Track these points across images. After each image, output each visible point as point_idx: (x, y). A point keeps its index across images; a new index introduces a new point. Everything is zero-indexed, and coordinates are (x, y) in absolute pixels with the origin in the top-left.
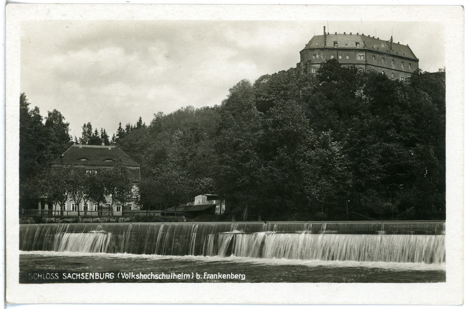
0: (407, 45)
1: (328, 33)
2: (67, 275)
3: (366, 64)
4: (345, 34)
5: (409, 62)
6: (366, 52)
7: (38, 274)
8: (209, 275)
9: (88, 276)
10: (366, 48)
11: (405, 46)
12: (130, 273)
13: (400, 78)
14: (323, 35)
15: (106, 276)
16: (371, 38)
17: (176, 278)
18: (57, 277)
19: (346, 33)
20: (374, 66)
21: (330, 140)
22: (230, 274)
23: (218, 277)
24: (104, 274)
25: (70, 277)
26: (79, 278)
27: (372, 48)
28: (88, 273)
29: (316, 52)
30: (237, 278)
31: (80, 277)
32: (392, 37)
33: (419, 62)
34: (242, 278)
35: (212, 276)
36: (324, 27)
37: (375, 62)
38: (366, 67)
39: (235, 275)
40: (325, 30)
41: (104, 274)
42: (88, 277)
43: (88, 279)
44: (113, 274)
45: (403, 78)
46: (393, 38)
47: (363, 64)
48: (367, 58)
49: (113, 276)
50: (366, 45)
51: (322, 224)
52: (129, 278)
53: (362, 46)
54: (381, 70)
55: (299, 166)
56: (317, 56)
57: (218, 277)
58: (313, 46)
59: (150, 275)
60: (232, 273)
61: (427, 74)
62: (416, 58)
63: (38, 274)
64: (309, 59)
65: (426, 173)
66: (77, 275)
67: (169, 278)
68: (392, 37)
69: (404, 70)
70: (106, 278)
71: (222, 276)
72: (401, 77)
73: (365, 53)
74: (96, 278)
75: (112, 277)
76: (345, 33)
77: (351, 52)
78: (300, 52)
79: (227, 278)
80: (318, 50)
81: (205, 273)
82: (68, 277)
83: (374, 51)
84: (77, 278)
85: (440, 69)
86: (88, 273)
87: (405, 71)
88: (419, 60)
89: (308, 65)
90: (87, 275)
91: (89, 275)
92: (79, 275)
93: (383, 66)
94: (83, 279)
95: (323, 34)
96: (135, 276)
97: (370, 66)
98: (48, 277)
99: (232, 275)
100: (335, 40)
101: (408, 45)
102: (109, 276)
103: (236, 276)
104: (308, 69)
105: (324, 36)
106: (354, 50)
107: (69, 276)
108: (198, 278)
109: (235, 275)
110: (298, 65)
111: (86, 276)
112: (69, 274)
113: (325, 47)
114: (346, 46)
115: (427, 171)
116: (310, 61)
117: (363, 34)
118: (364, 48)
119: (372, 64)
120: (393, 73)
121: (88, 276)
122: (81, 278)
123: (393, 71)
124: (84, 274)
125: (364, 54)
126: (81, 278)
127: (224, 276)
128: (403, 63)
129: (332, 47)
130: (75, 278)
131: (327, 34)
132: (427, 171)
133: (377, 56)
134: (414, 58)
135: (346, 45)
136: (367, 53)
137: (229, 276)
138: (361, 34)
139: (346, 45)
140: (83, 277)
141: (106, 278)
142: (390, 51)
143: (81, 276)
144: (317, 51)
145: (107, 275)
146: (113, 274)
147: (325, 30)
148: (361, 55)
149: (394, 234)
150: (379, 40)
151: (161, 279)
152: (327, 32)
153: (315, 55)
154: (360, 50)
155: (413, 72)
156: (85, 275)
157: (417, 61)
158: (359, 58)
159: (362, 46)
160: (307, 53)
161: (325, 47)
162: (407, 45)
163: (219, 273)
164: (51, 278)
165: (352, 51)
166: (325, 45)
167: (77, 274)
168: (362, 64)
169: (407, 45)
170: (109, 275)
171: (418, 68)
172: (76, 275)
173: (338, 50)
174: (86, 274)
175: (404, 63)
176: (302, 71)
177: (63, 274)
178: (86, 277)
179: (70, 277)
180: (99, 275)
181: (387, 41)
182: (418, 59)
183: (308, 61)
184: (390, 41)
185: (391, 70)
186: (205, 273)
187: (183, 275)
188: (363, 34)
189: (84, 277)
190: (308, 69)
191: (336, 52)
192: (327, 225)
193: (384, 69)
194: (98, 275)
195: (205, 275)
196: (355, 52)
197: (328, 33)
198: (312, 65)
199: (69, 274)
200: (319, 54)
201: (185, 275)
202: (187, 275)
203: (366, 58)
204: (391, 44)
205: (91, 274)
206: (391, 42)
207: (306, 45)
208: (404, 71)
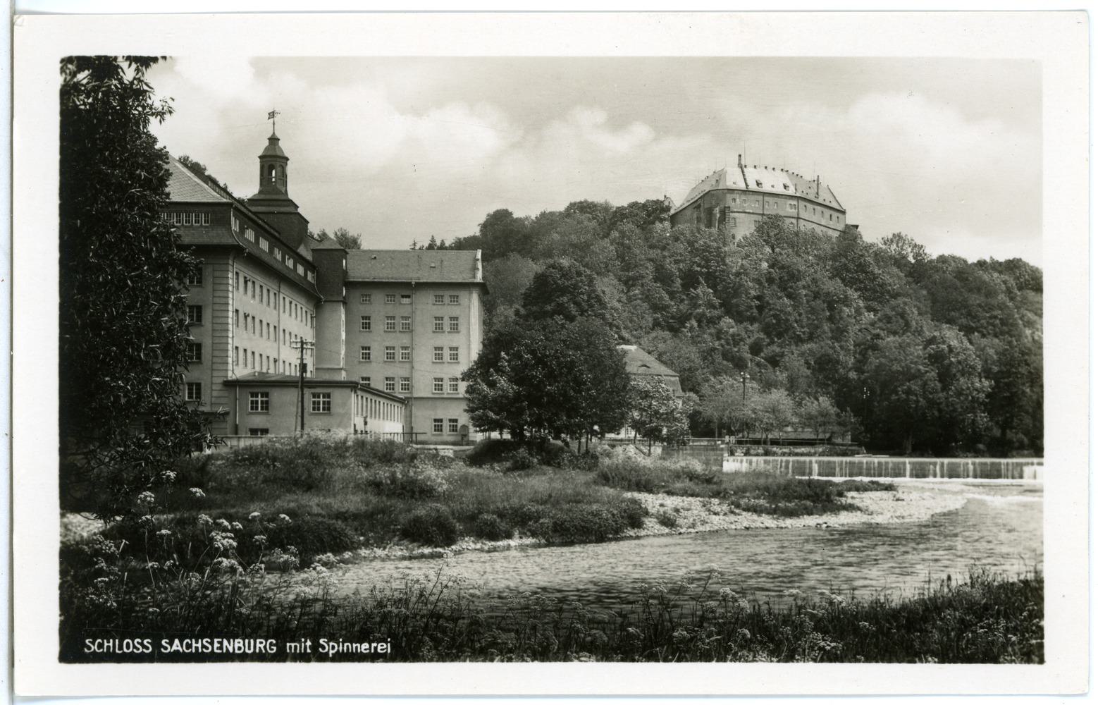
2: (171, 644)
7: (105, 641)
15: (258, 645)
18: (148, 648)
25: (180, 648)
26: (200, 651)
28: (220, 640)
30: (368, 651)
31: (202, 648)
36: (740, 156)
40: (740, 160)
42: (221, 648)
43: (219, 651)
49: (275, 648)
52: (338, 650)
63: (105, 641)
70: (257, 651)
74: (237, 651)
84: (194, 651)
86: (220, 640)
91: (221, 643)
92: (199, 645)
102: (265, 647)
111: (216, 645)
112: (177, 641)
122: (204, 650)
124: (140, 641)
126: (204, 650)
130: (101, 650)
135: (773, 186)
137: (357, 647)
139: (773, 186)
140: (207, 648)
143: (203, 646)
147: (740, 160)
149: (353, 547)
153: (734, 200)
154: (791, 197)
164: (135, 651)
167: (194, 640)
168: (793, 218)
172: (192, 644)
173: (764, 194)
174: (216, 640)
177: (87, 641)
179: (180, 648)
187: (343, 646)
189: (210, 647)
191: (760, 198)
194: (241, 645)
199: (177, 641)
201: (346, 645)
205: (225, 643)
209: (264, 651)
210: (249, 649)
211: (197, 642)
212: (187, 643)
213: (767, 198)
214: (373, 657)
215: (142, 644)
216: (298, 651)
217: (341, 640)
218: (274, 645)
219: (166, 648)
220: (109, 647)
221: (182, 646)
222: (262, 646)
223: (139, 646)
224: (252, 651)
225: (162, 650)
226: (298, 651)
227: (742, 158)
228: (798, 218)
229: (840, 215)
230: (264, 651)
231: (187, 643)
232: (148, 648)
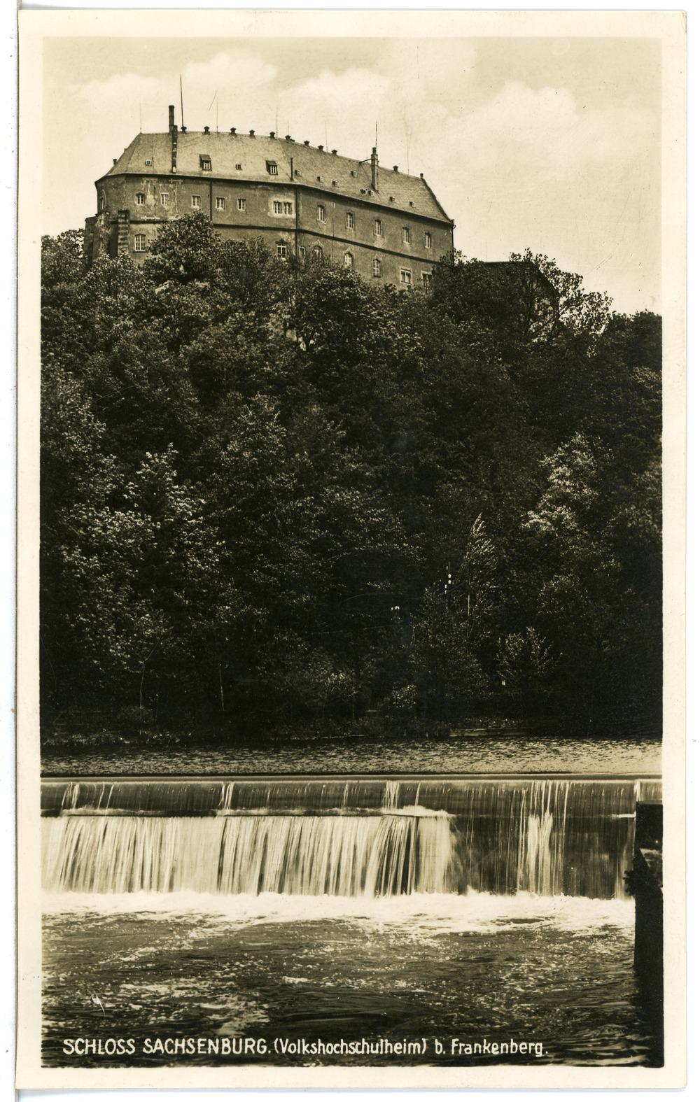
0: (422, 175)
1: (184, 128)
2: (153, 1044)
3: (299, 232)
4: (236, 135)
5: (425, 228)
6: (296, 194)
8: (464, 1045)
9: (203, 1045)
10: (297, 182)
11: (416, 179)
12: (299, 1041)
13: (401, 276)
14: (169, 134)
15: (247, 1046)
16: (314, 149)
17: (391, 1052)
18: (130, 1049)
19: (236, 132)
20: (322, 236)
21: (168, 479)
22: (509, 1043)
23: (482, 1049)
24: (241, 1040)
25: (161, 1047)
27: (315, 180)
28: (205, 1040)
29: (146, 187)
32: (374, 150)
33: (457, 232)
34: (537, 1052)
35: (470, 1049)
36: (171, 108)
37: (325, 227)
38: (298, 240)
39: (519, 1045)
40: (172, 117)
41: (241, 1040)
44: (265, 1041)
45: (409, 275)
46: (377, 152)
47: (289, 230)
48: (301, 213)
50: (296, 171)
51: (63, 789)
52: (297, 1052)
53: (287, 174)
54: (344, 249)
55: (71, 566)
56: (150, 198)
57: (482, 1049)
58: (137, 166)
59: (338, 1045)
60: (512, 1040)
61: (477, 266)
62: (447, 218)
64: (124, 208)
65: (448, 585)
66: (177, 1045)
67: (503, 1045)
68: (374, 150)
69: (412, 250)
70: (246, 1052)
71: (490, 1049)
72: (403, 274)
73: (292, 195)
75: (261, 1049)
76: (233, 130)
77: (253, 192)
78: (96, 183)
79: (405, 1052)
80: (153, 179)
81: (454, 1041)
82: (156, 1048)
83: (323, 192)
84: (176, 1052)
85: (514, 255)
86: (205, 1040)
87: (415, 255)
88: (455, 223)
89: (120, 226)
90: (202, 1042)
92: (183, 1045)
93: (348, 239)
94: (130, 1053)
95: (166, 129)
96: (309, 1048)
97: (310, 237)
98: (110, 1049)
99: (513, 1044)
100: (205, 152)
101: (424, 178)
102: (255, 1048)
103: (396, 1048)
104: (122, 239)
105: (171, 137)
106: (260, 186)
107: (159, 1045)
108: (439, 1050)
109: (519, 1045)
110: (90, 222)
111: (200, 1045)
112: (159, 1041)
113: (172, 171)
114: (238, 172)
115: (450, 576)
116: (127, 212)
117: (288, 137)
118: (292, 179)
119: (316, 231)
120: (379, 261)
121: (203, 1045)
122: (188, 1051)
123: (380, 256)
124: (193, 1040)
125: (292, 201)
127: (397, 1048)
128: (408, 230)
129: (195, 173)
131: (179, 129)
132: (450, 576)
133: (331, 205)
134: (441, 218)
135: (239, 167)
136: (302, 196)
138: (281, 135)
139: (239, 167)
140: (191, 1050)
141: (246, 1052)
142: (370, 192)
143: (187, 1047)
144: (148, 182)
145: (250, 1043)
146: (265, 1041)
147: (172, 117)
148: (281, 200)
150: (338, 157)
151: (338, 1052)
152: (178, 122)
153: (142, 196)
154: (280, 188)
155: (437, 259)
156: (196, 1045)
157: (449, 226)
158: (273, 213)
159: (287, 174)
160: (118, 186)
161: (172, 171)
162: (422, 175)
163: (485, 1040)
165: (254, 189)
166: (174, 164)
168: (284, 230)
169: (419, 176)
170: (253, 1045)
171: (454, 250)
172: (85, 1044)
175: (411, 231)
176: (102, 245)
177: (146, 1042)
178: (199, 1048)
179: (161, 1047)
180: (231, 1045)
181: (360, 163)
182: (452, 221)
183: (120, 212)
184: (370, 162)
185: (372, 251)
186: (454, 1041)
188: (288, 137)
190: (120, 237)
191: (205, 188)
192: (82, 789)
193: (353, 246)
194: (228, 1045)
195: (454, 1045)
196: (265, 193)
197: (184, 128)
198: (134, 226)
199: (159, 1041)
200: (155, 192)
201: (410, 1045)
202: (414, 1045)
203: (297, 211)
204: (373, 170)
206: (373, 166)
207: (115, 160)
208: (410, 255)
209: (253, 1052)
210: (237, 1049)
211: (180, 1043)
212: (80, 1042)
213: (216, 189)
214: (526, 1059)
215: (125, 1044)
216: (414, 1052)
217: (405, 1040)
218: (264, 1044)
219: (148, 1049)
220: (91, 1049)
221: (164, 1046)
222: (251, 1047)
223: (123, 1047)
224: (240, 1052)
225: (65, 1050)
226: (414, 1052)
227: (177, 112)
228: (299, 232)
229: (439, 233)
230: (253, 1052)
231: (80, 1042)
232: (130, 1049)
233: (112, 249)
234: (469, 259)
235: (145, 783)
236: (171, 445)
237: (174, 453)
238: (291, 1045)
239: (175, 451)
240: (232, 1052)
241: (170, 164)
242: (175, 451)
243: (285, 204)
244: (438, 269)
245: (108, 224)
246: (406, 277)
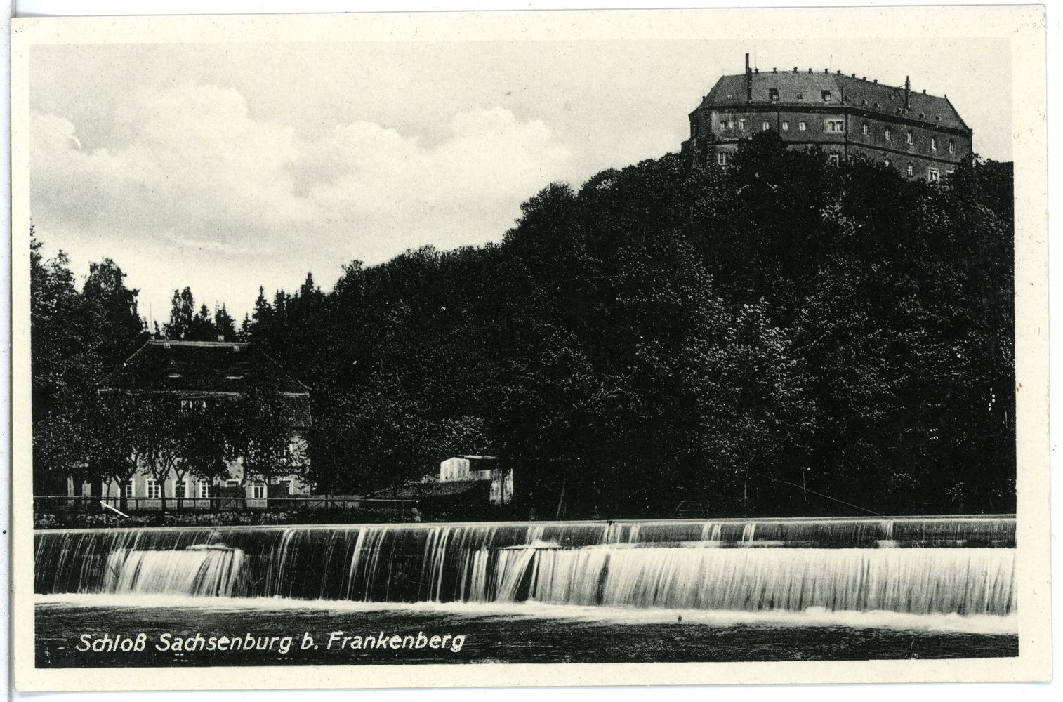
17: (372, 646)
36: (747, 55)
40: (747, 62)
46: (909, 80)
53: (838, 100)
68: (908, 77)
69: (939, 155)
72: (931, 173)
78: (690, 115)
88: (973, 132)
99: (248, 638)
104: (709, 156)
114: (800, 100)
131: (753, 71)
132: (994, 396)
134: (961, 127)
147: (747, 62)
152: (752, 66)
155: (959, 160)
159: (838, 100)
182: (971, 130)
188: (839, 72)
197: (757, 70)
198: (718, 146)
224: (264, 648)
225: (157, 646)
233: (703, 161)
234: (985, 159)
235: (843, 522)
236: (763, 298)
237: (766, 304)
238: (125, 641)
239: (766, 302)
240: (133, 648)
241: (746, 97)
242: (766, 302)
243: (837, 122)
244: (959, 168)
245: (698, 146)
246: (934, 176)
